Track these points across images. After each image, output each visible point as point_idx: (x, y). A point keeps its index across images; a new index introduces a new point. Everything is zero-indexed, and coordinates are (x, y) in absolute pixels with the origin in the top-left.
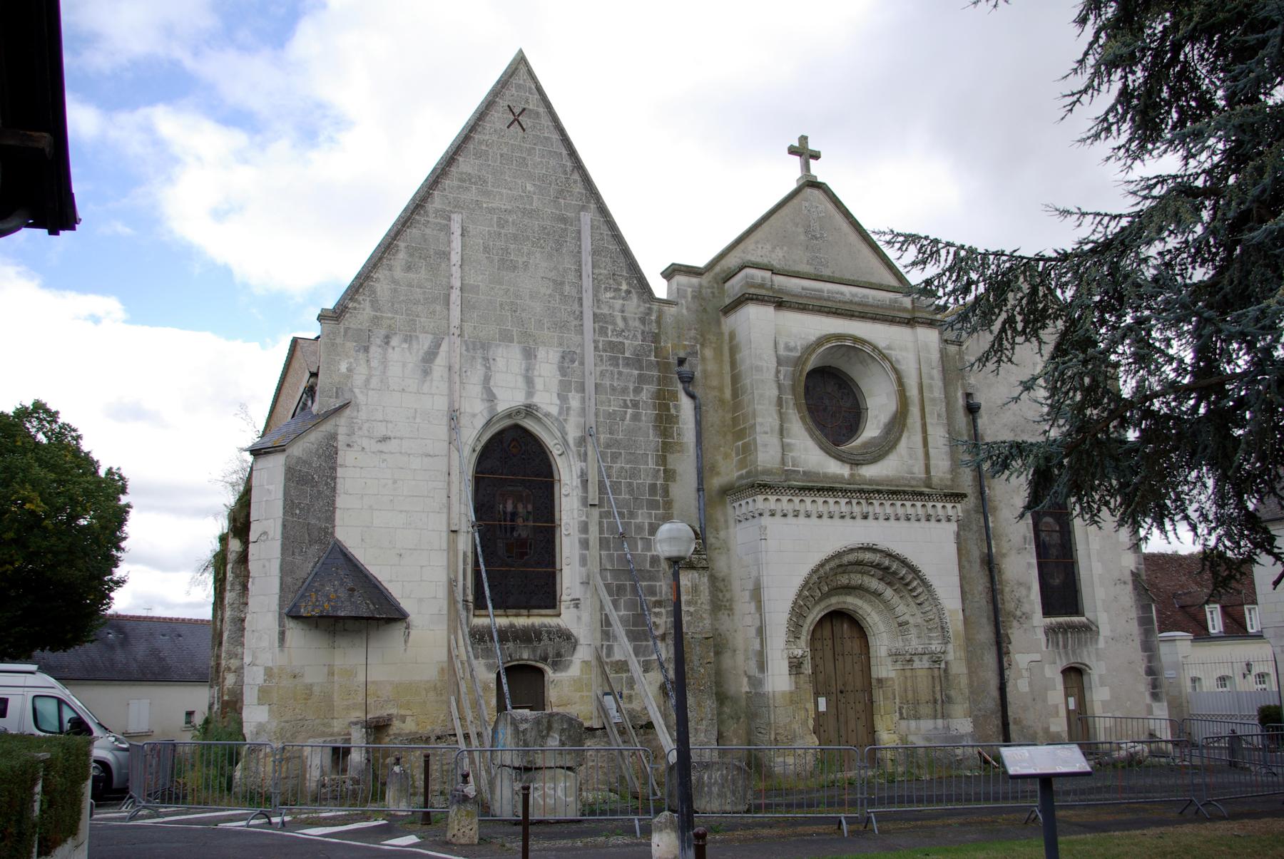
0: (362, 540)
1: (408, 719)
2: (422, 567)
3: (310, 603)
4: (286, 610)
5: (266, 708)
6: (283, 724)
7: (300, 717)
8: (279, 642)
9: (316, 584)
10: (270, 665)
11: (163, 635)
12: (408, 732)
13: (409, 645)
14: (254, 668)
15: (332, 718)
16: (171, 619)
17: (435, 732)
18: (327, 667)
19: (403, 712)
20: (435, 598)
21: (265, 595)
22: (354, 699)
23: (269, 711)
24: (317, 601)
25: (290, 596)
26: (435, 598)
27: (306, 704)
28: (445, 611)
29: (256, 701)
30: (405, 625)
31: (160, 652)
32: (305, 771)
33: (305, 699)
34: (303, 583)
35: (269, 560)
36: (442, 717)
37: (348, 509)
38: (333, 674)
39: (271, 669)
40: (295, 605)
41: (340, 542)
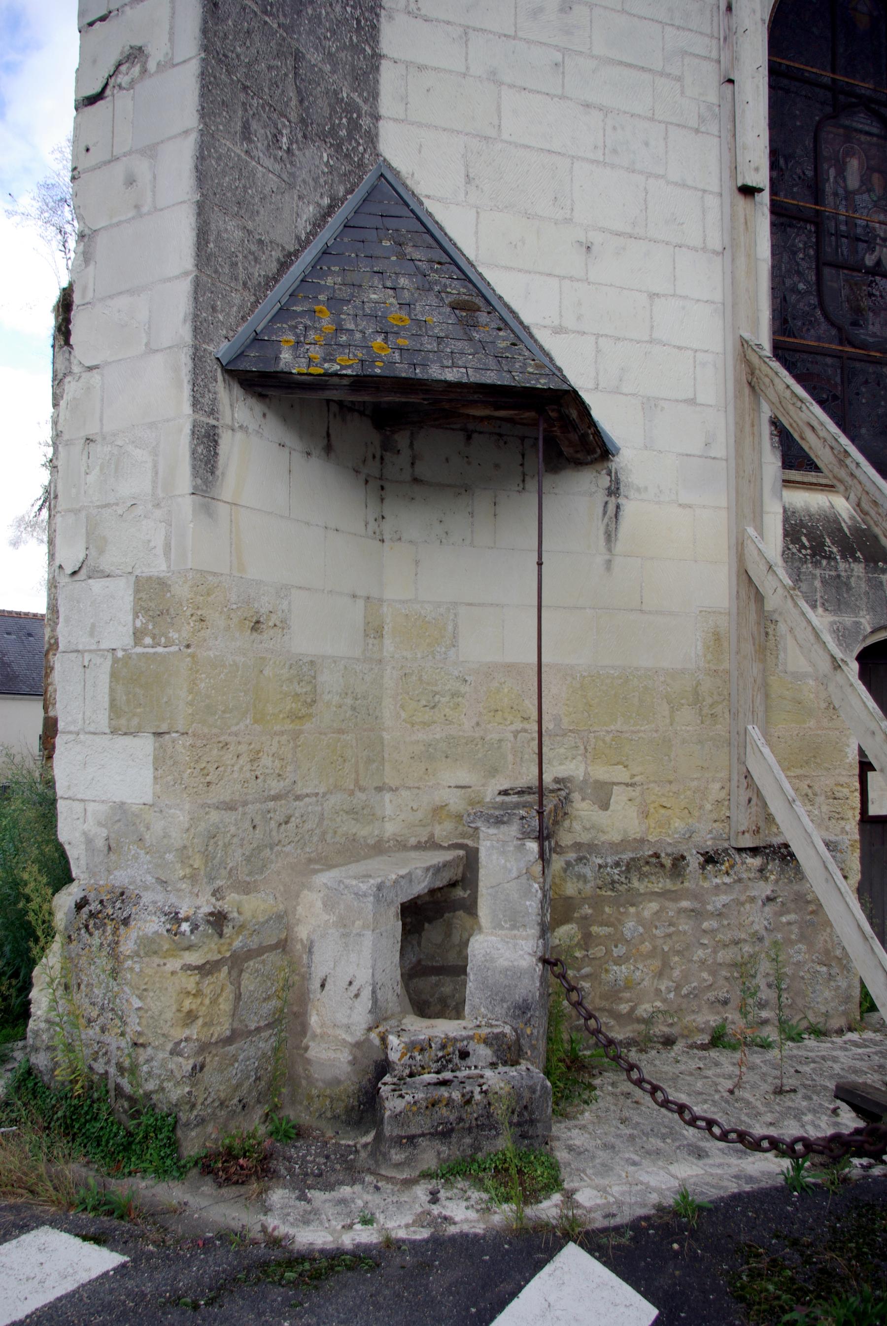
0: (468, 179)
1: (619, 796)
2: (653, 296)
3: (312, 336)
4: (221, 348)
5: (145, 745)
6: (214, 816)
7: (275, 786)
8: (195, 473)
9: (330, 281)
10: (159, 567)
11: (9, 634)
12: (616, 838)
13: (619, 547)
14: (97, 585)
15: (379, 789)
16: (19, 614)
17: (696, 838)
18: (361, 603)
19: (601, 772)
20: (692, 402)
21: (130, 292)
22: (448, 721)
23: (158, 762)
24: (339, 329)
25: (236, 298)
26: (692, 402)
27: (296, 735)
28: (720, 449)
29: (102, 720)
30: (605, 481)
31: (4, 655)
32: (303, 999)
33: (295, 717)
34: (284, 266)
35: (150, 151)
36: (715, 791)
37: (421, 68)
38: (379, 633)
39: (162, 584)
40: (257, 339)
41: (397, 174)
